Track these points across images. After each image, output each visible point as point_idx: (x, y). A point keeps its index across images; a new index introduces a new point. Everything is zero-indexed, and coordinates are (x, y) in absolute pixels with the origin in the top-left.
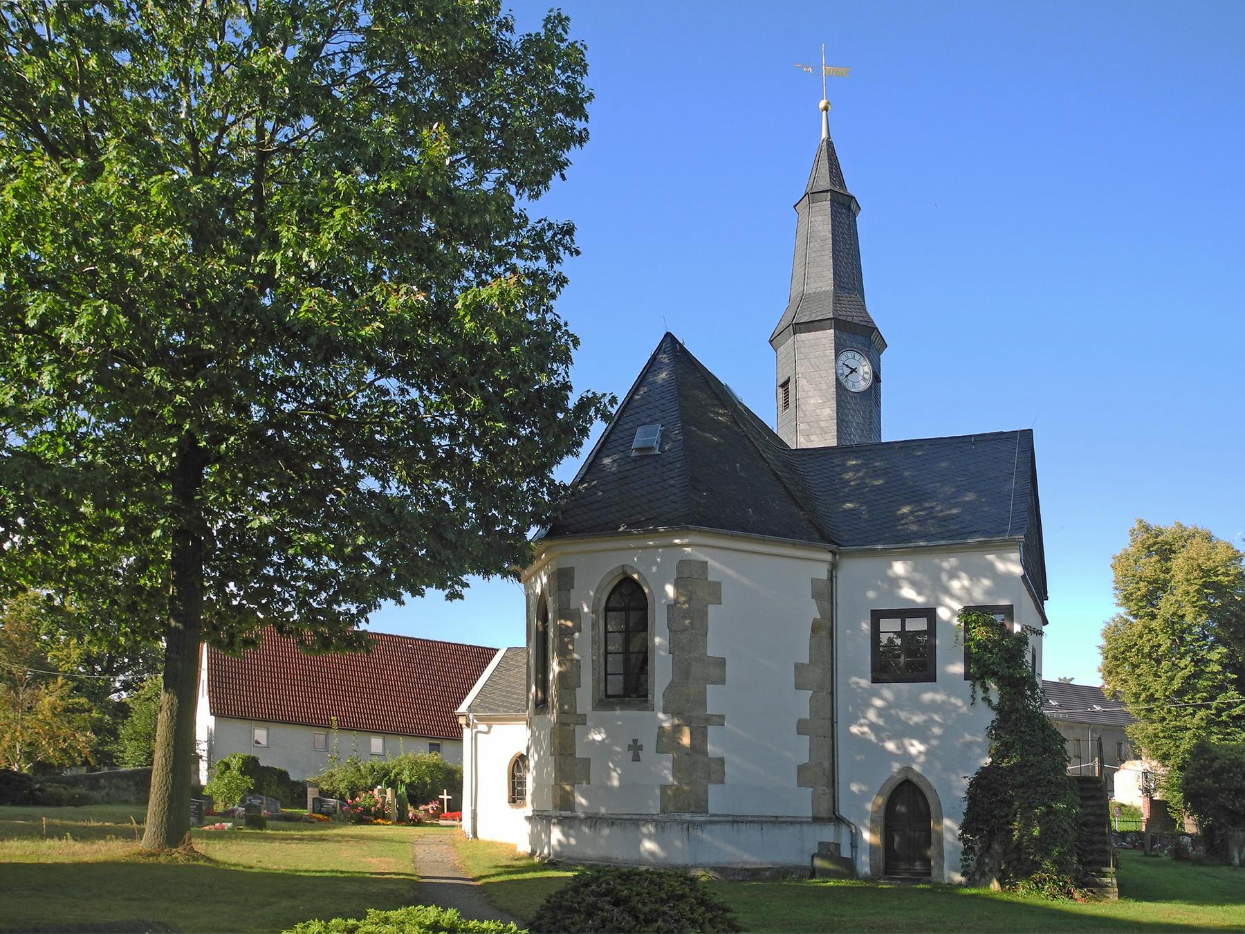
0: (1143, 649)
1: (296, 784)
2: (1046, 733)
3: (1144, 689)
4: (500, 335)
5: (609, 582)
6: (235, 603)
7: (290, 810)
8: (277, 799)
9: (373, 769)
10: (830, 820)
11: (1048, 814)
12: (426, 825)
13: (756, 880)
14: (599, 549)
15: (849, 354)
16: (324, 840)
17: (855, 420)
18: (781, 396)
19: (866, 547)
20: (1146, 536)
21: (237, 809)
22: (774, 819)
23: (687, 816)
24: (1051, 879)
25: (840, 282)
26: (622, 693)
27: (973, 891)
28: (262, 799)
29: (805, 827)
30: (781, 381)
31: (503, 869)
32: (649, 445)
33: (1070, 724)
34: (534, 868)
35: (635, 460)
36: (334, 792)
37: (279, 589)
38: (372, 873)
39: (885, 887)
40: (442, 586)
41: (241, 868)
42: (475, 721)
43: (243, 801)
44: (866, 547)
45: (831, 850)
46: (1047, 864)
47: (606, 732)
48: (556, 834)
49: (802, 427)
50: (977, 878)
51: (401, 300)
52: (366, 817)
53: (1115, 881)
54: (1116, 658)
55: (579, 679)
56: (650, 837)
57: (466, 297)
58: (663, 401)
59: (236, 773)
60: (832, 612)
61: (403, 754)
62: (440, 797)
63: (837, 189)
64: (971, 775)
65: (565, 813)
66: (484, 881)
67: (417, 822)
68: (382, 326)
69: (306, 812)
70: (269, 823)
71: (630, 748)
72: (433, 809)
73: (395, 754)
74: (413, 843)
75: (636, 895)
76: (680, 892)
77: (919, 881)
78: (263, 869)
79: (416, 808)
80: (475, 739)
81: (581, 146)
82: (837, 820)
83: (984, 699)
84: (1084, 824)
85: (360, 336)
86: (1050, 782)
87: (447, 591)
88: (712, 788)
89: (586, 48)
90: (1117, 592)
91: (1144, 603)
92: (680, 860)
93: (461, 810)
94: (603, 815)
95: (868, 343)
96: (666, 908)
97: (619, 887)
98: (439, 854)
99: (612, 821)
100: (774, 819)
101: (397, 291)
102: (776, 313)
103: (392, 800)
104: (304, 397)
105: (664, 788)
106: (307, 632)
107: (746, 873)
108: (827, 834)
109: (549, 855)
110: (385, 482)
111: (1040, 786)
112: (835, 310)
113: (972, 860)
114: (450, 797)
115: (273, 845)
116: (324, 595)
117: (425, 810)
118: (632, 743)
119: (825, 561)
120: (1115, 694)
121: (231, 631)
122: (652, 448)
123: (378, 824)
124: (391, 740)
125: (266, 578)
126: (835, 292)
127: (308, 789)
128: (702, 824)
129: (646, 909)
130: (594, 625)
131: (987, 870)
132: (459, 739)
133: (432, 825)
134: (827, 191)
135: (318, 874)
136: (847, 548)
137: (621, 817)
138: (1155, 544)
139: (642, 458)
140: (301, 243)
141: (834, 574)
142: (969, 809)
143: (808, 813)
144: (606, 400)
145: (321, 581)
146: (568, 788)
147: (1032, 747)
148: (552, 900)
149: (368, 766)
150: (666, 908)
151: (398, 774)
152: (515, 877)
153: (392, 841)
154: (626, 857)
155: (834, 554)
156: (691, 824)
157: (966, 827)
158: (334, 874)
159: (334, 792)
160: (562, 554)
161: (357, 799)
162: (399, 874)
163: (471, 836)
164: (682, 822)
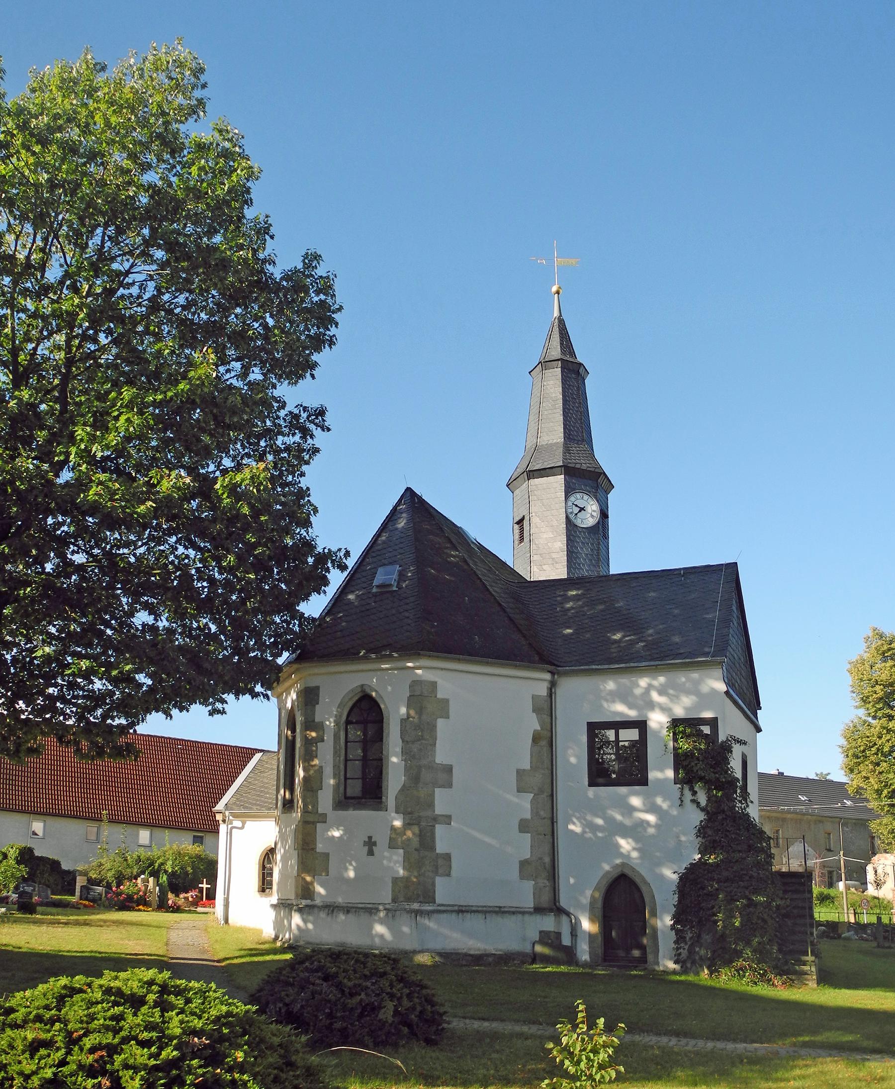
0: (883, 748)
1: (68, 872)
2: (751, 832)
3: (885, 786)
4: (252, 507)
5: (351, 699)
6: (23, 717)
7: (59, 897)
8: (48, 886)
9: (139, 860)
10: (551, 910)
11: (749, 906)
12: (183, 911)
13: (481, 965)
14: (342, 670)
15: (578, 496)
16: (87, 924)
17: (584, 552)
18: (517, 531)
19: (582, 667)
20: (880, 643)
21: (11, 896)
22: (498, 909)
23: (416, 906)
24: (751, 967)
25: (569, 435)
26: (360, 795)
27: (683, 978)
28: (34, 887)
29: (527, 917)
30: (517, 519)
31: (246, 952)
32: (387, 583)
33: (820, 818)
34: (275, 951)
35: (375, 595)
36: (101, 881)
37: (62, 706)
38: (127, 954)
39: (600, 972)
40: (205, 703)
41: (10, 948)
42: (231, 818)
43: (16, 888)
44: (582, 667)
45: (552, 938)
46: (748, 952)
47: (345, 830)
48: (297, 919)
49: (535, 558)
50: (689, 965)
51: (171, 483)
52: (128, 903)
53: (813, 969)
54: (858, 757)
55: (321, 783)
56: (381, 922)
57: (224, 480)
58: (402, 546)
59: (12, 862)
60: (552, 724)
61: (168, 846)
62: (200, 885)
63: (568, 358)
64: (682, 867)
65: (304, 902)
66: (228, 962)
67: (176, 909)
68: (154, 505)
69: (74, 899)
70: (39, 909)
71: (365, 843)
72: (192, 897)
73: (161, 845)
74: (168, 928)
75: (343, 972)
76: (382, 970)
77: (635, 968)
78: (30, 949)
79: (177, 896)
80: (230, 834)
81: (331, 348)
82: (559, 911)
83: (693, 801)
84: (786, 916)
85: (136, 513)
86: (751, 877)
87: (210, 708)
88: (439, 881)
89: (336, 277)
90: (854, 695)
91: (881, 705)
92: (408, 945)
93: (215, 899)
94: (340, 903)
95: (596, 485)
96: (369, 984)
97: (328, 965)
98: (190, 938)
99: (347, 909)
100: (498, 909)
101: (169, 475)
102: (513, 463)
103: (154, 888)
104: (92, 548)
105: (395, 880)
106: (85, 744)
107: (470, 958)
108: (548, 923)
109: (290, 939)
110: (157, 617)
111: (743, 881)
112: (565, 459)
113: (684, 949)
114: (209, 886)
115: (42, 928)
116: (99, 712)
117: (185, 898)
118: (367, 840)
119: (545, 680)
120: (859, 790)
121: (18, 741)
122: (390, 585)
123: (140, 910)
124: (158, 832)
125: (50, 697)
126: (565, 443)
127: (78, 878)
128: (429, 913)
129: (350, 984)
130: (336, 736)
131: (697, 958)
132: (217, 832)
133: (190, 912)
134: (558, 360)
135: (78, 954)
136: (565, 668)
137: (356, 905)
138: (889, 650)
139: (382, 593)
140: (93, 439)
141: (553, 690)
142: (680, 901)
143: (530, 904)
144: (342, 554)
145: (97, 699)
146: (308, 879)
147: (737, 844)
148: (272, 975)
149: (135, 856)
150: (369, 984)
151: (162, 864)
152: (256, 959)
153: (149, 926)
154: (359, 943)
155: (553, 673)
156: (417, 913)
157: (677, 918)
158: (93, 954)
159: (101, 881)
160: (310, 675)
161: (122, 887)
162: (151, 955)
163: (223, 922)
164: (411, 911)
